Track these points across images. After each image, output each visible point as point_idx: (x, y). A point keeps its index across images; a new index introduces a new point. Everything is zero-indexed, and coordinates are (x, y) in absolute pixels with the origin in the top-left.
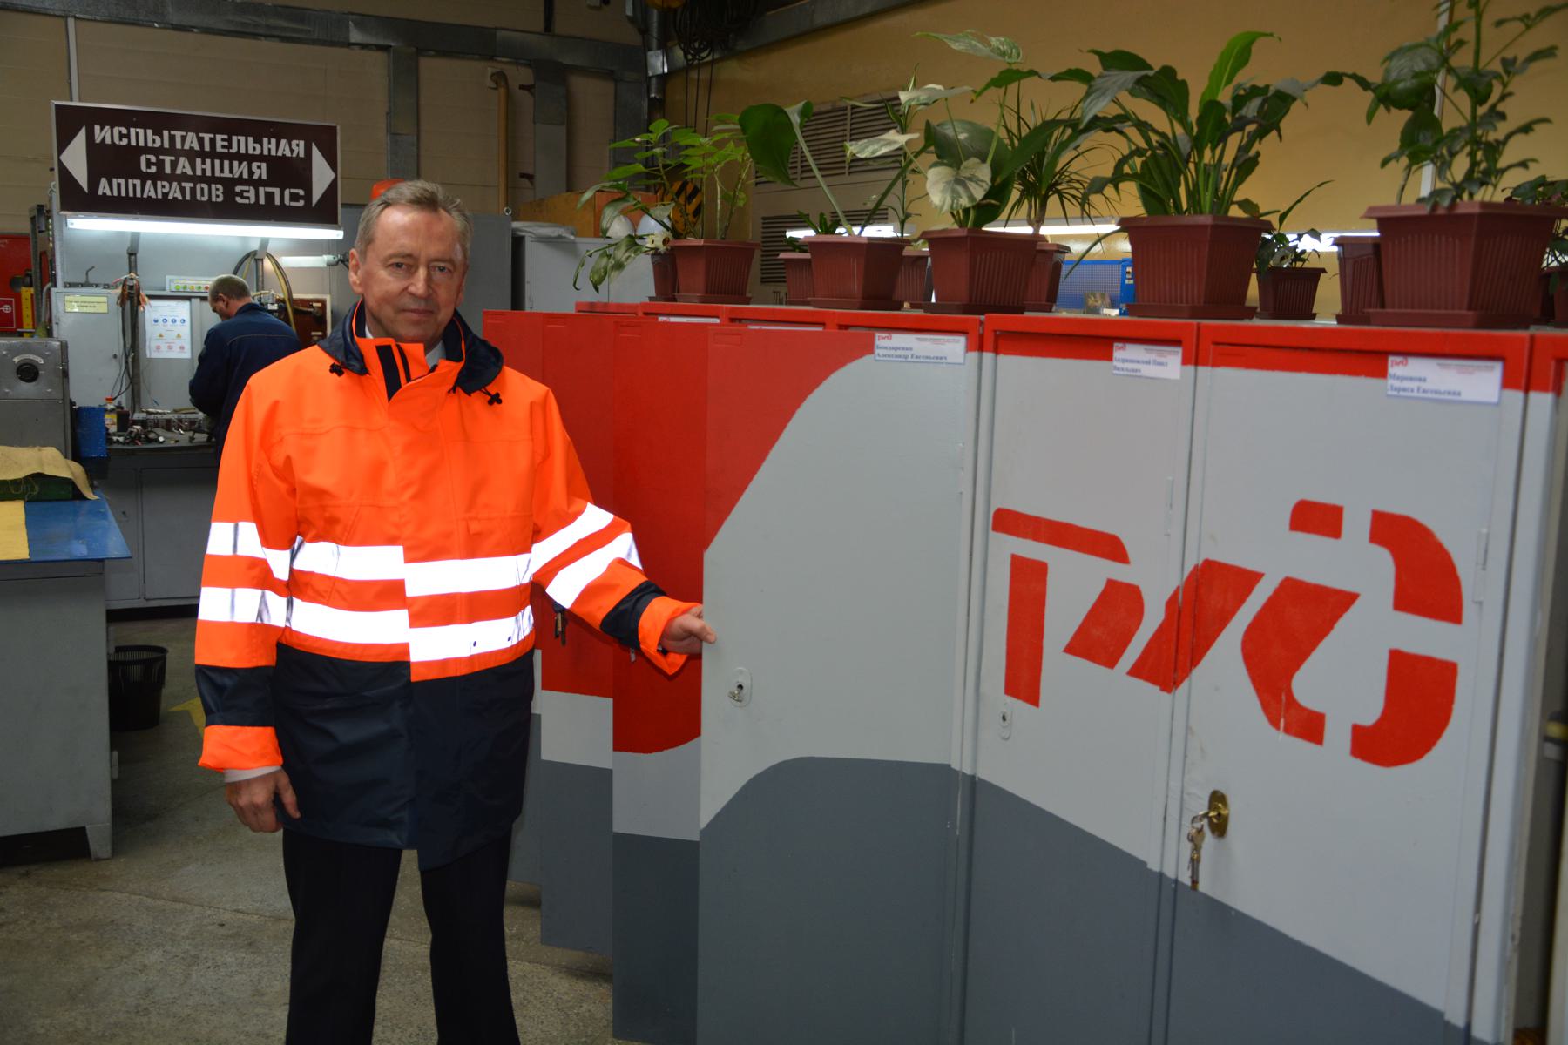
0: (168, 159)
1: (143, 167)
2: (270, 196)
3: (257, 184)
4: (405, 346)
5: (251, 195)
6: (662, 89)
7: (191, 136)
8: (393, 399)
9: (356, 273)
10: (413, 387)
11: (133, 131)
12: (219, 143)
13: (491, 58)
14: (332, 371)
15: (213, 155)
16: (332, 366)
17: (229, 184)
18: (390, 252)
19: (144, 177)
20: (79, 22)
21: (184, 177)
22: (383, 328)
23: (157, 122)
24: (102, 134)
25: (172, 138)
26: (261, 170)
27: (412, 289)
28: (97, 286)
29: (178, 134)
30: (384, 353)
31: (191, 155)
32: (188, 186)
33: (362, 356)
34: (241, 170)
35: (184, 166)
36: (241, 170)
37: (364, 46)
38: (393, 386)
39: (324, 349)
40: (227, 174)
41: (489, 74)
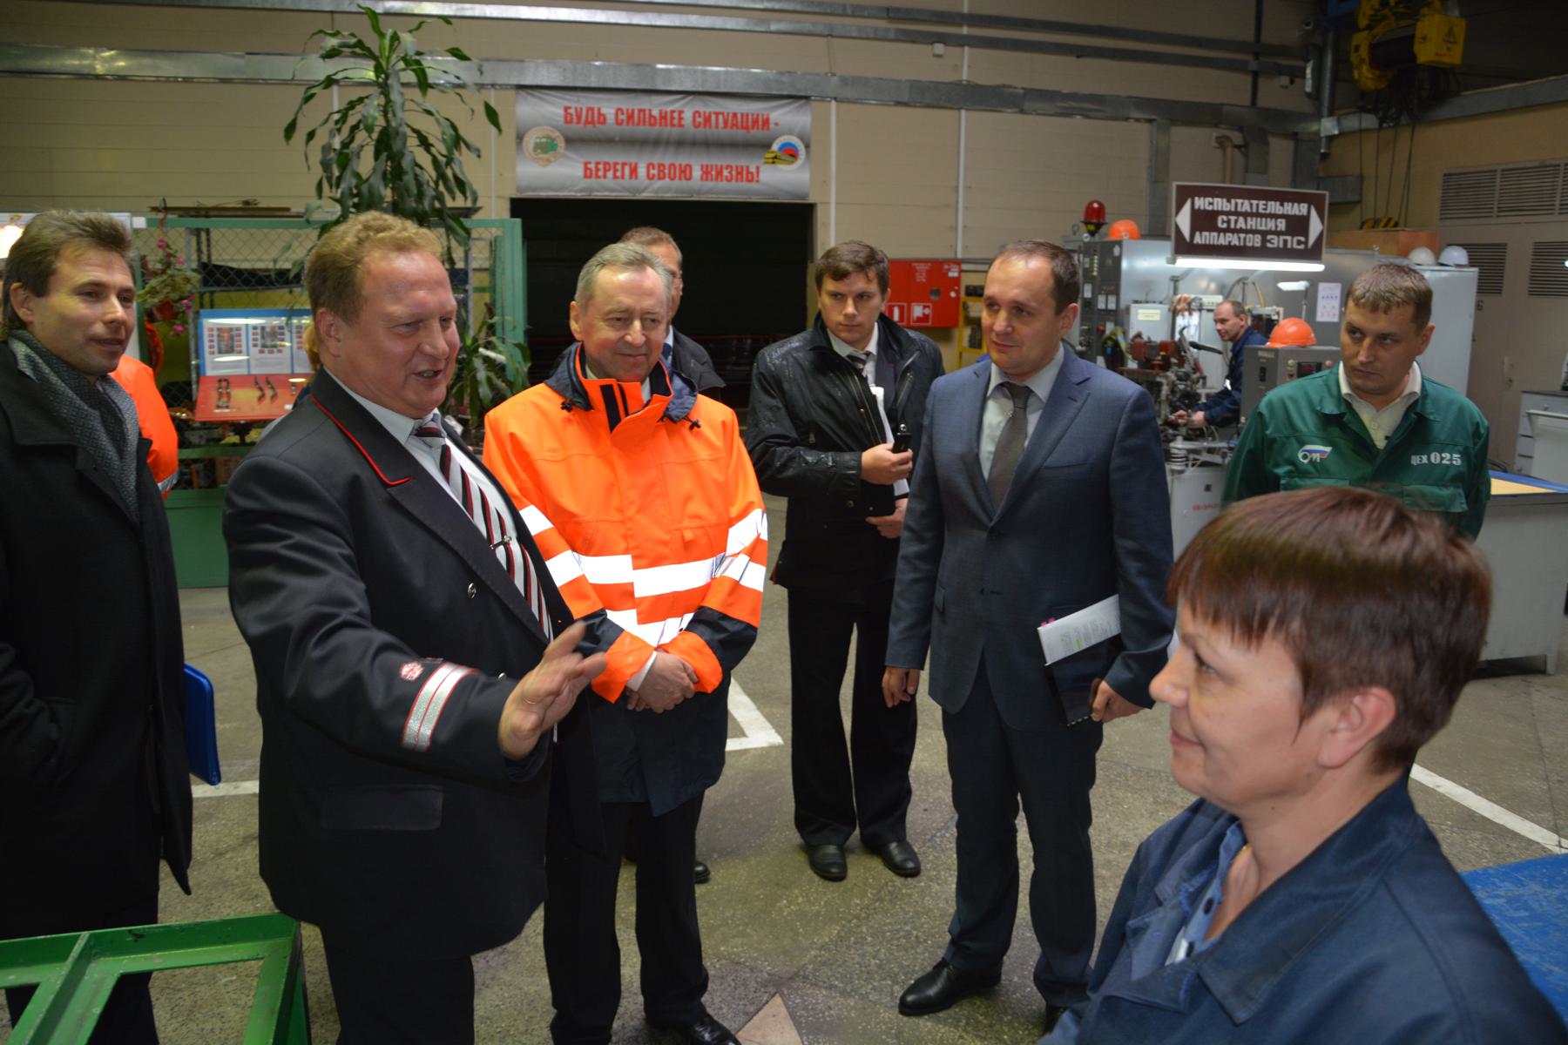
0: (1233, 218)
1: (1220, 225)
2: (1285, 242)
3: (1278, 233)
4: (623, 384)
5: (1275, 242)
6: (1328, 147)
7: (1246, 202)
8: (615, 430)
9: (577, 323)
10: (629, 421)
11: (1216, 200)
12: (1261, 207)
13: (1216, 126)
14: (563, 408)
15: (1257, 215)
16: (563, 404)
17: (1264, 234)
18: (609, 308)
19: (1220, 231)
20: (845, 106)
21: (1241, 231)
22: (601, 372)
23: (1228, 194)
24: (1202, 203)
25: (1236, 204)
26: (1282, 224)
27: (629, 338)
28: (1154, 302)
29: (1240, 201)
30: (607, 391)
31: (1246, 215)
32: (1242, 236)
33: (586, 393)
34: (1270, 224)
35: (1241, 224)
36: (1270, 224)
37: (1137, 120)
38: (614, 420)
39: (549, 386)
40: (1263, 228)
41: (1214, 137)
